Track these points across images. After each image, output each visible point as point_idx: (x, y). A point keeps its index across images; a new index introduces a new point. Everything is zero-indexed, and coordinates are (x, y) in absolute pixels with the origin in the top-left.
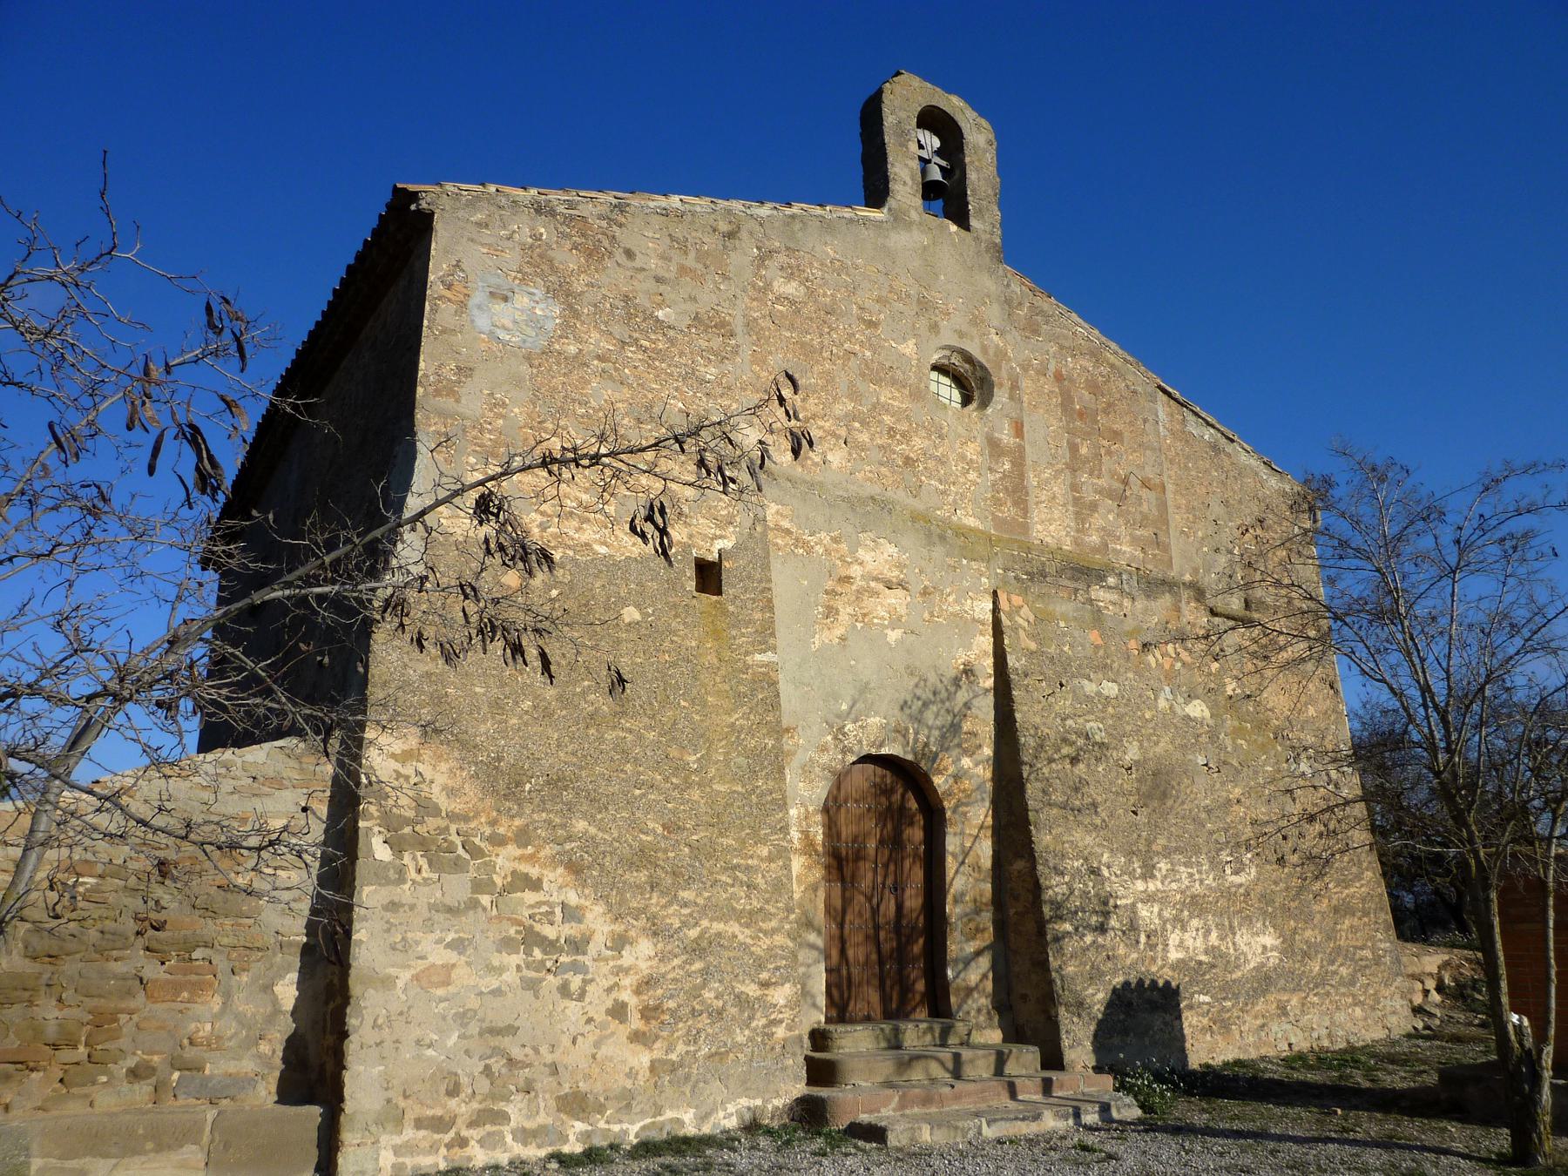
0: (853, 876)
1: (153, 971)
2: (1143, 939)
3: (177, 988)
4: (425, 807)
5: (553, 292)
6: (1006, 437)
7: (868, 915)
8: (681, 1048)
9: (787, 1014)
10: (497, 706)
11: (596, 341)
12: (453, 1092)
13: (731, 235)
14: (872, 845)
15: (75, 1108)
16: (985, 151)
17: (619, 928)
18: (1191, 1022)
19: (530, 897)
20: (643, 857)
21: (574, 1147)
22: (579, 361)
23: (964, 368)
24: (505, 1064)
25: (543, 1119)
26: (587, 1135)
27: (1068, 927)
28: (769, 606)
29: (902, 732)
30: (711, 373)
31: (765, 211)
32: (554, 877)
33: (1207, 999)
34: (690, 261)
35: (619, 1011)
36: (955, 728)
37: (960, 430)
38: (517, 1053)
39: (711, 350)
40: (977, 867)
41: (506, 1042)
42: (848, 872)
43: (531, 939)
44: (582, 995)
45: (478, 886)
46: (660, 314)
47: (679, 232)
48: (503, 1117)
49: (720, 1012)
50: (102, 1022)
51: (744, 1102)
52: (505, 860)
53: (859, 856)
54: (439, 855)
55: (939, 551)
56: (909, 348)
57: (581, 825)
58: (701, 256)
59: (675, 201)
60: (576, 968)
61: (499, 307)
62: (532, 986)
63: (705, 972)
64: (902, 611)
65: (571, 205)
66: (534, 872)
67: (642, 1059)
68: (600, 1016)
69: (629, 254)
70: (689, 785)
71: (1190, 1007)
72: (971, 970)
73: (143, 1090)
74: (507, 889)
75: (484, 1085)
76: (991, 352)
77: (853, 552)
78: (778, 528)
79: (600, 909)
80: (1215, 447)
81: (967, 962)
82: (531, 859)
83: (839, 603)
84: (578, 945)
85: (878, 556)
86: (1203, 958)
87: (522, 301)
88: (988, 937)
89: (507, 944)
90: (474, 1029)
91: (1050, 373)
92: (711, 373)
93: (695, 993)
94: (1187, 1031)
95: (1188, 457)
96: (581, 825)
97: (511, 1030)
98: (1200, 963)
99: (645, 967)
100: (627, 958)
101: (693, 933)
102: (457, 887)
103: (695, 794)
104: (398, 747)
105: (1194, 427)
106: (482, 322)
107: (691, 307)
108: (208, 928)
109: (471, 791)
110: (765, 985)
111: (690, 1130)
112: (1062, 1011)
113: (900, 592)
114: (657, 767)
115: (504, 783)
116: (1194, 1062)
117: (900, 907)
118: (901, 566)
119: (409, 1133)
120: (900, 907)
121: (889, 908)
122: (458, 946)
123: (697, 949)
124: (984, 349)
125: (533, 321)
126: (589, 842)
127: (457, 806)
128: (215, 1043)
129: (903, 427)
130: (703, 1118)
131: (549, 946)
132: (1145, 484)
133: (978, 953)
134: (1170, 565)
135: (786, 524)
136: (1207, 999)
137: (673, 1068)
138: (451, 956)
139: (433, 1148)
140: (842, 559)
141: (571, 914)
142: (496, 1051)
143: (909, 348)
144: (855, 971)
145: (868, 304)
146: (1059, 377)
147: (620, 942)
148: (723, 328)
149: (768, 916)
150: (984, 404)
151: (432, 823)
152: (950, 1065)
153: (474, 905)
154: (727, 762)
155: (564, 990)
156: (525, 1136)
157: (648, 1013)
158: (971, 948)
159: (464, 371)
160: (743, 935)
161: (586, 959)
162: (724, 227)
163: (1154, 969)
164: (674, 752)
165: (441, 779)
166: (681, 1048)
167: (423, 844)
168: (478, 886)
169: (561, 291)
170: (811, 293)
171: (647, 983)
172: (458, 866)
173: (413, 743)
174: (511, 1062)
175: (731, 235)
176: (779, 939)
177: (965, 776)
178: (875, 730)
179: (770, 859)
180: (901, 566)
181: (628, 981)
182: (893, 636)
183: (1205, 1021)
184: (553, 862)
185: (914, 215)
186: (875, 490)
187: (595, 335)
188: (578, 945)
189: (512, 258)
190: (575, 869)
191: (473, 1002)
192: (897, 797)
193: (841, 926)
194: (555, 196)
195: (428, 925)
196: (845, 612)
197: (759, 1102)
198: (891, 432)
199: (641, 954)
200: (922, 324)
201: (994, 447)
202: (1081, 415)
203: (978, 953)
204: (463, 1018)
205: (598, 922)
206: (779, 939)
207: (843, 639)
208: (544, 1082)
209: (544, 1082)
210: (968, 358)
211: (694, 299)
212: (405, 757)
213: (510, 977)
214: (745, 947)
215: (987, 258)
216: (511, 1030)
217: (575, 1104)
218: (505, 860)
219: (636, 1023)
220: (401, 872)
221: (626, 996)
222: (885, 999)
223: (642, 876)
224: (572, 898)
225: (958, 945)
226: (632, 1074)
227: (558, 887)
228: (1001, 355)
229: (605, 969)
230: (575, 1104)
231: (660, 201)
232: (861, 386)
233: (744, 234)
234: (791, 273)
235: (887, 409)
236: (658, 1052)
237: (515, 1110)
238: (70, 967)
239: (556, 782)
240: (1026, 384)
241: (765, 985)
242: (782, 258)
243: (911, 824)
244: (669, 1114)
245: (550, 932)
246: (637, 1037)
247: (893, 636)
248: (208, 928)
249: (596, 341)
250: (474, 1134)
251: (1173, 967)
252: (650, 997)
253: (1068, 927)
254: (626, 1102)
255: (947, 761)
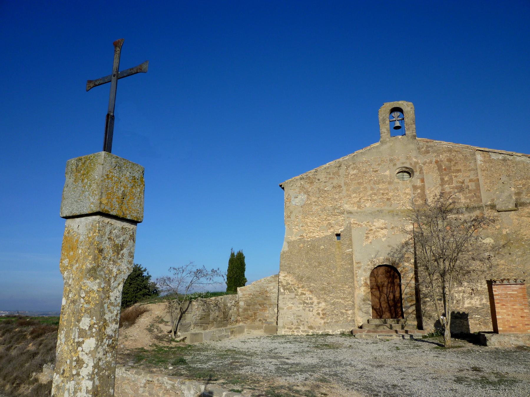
0: (382, 290)
1: (260, 307)
2: (455, 302)
3: (263, 310)
4: (288, 284)
5: (305, 193)
6: (419, 183)
7: (386, 298)
8: (330, 320)
9: (351, 315)
10: (299, 267)
11: (314, 199)
12: (292, 324)
13: (340, 166)
14: (386, 283)
15: (253, 324)
16: (410, 111)
17: (319, 301)
18: (471, 322)
19: (304, 296)
20: (323, 289)
21: (310, 334)
22: (311, 204)
23: (407, 170)
24: (300, 322)
25: (306, 329)
26: (312, 332)
27: (428, 299)
28: (351, 240)
29: (388, 259)
30: (337, 197)
31: (347, 158)
32: (308, 293)
33: (479, 316)
34: (331, 176)
35: (319, 314)
36: (403, 257)
37: (404, 187)
38: (302, 320)
39: (337, 192)
40: (410, 287)
41: (300, 318)
42: (381, 289)
43: (304, 303)
44: (312, 311)
45: (296, 295)
46: (326, 189)
47: (328, 171)
48: (300, 328)
49: (337, 315)
50: (255, 314)
51: (341, 330)
52: (300, 291)
53: (383, 286)
54: (290, 290)
55: (396, 218)
56: (387, 173)
57: (312, 284)
58: (333, 174)
59: (327, 165)
60: (312, 307)
61: (296, 199)
62: (304, 310)
63: (335, 308)
64: (386, 233)
65: (307, 175)
66: (305, 292)
67: (322, 321)
68: (315, 314)
69: (319, 180)
70: (332, 276)
71: (472, 318)
72: (409, 309)
73: (260, 323)
74: (301, 295)
75: (297, 324)
76: (413, 164)
77: (372, 223)
78: (354, 223)
79: (315, 298)
80: (504, 160)
81: (409, 307)
82: (304, 290)
83: (369, 235)
84: (312, 303)
85: (379, 223)
86: (479, 306)
87: (300, 197)
88: (414, 302)
89: (300, 303)
90: (295, 316)
91: (434, 162)
92: (337, 197)
93: (333, 311)
94: (470, 324)
95: (492, 167)
96: (312, 284)
97: (301, 316)
98: (477, 308)
99: (323, 307)
100: (320, 305)
101: (332, 301)
102: (293, 295)
103: (333, 277)
104: (284, 275)
105: (494, 156)
106: (294, 203)
107: (332, 185)
108: (265, 302)
109: (295, 280)
110: (347, 310)
111: (331, 333)
112: (424, 318)
113: (385, 230)
114: (326, 274)
115: (300, 279)
116: (472, 332)
117: (394, 296)
118: (385, 224)
119: (286, 329)
120: (394, 296)
121: (391, 296)
122: (293, 304)
123: (333, 304)
124: (411, 164)
125: (302, 200)
126: (314, 287)
127: (293, 283)
128: (268, 317)
129: (387, 192)
130: (333, 332)
131: (307, 304)
132: (471, 181)
133: (411, 305)
134: (481, 201)
135: (356, 222)
136: (479, 316)
137: (328, 323)
138: (292, 305)
139: (290, 332)
140: (370, 226)
141: (311, 299)
142: (299, 319)
143: (387, 173)
144: (383, 309)
145: (375, 167)
146: (437, 162)
147: (319, 303)
148: (340, 186)
149: (348, 298)
150: (413, 176)
151: (289, 286)
152: (389, 327)
153: (295, 298)
154: (340, 271)
155: (309, 310)
156: (303, 331)
157: (323, 314)
158: (409, 304)
159: (291, 213)
160: (342, 302)
161: (313, 306)
162: (338, 165)
163: (458, 309)
164: (330, 270)
165: (290, 279)
166: (330, 320)
167: (288, 289)
168: (296, 295)
169: (307, 193)
170: (360, 171)
171: (324, 310)
172: (293, 292)
173: (286, 274)
174: (301, 321)
175: (340, 166)
176: (350, 302)
177: (407, 267)
178: (381, 260)
179: (349, 288)
180: (385, 224)
181: (320, 309)
182: (383, 239)
183: (477, 322)
184: (308, 291)
185: (388, 140)
186: (379, 209)
187: (313, 198)
188: (312, 303)
189: (298, 190)
190: (311, 292)
191: (295, 312)
192: (392, 273)
193: (380, 300)
194: (304, 175)
195: (289, 301)
196: (371, 237)
197: (344, 330)
198: (383, 194)
199: (323, 305)
200: (391, 165)
201: (415, 188)
202: (445, 169)
203: (411, 305)
204: (294, 314)
205: (315, 300)
206: (350, 302)
207: (371, 242)
208: (306, 324)
209: (306, 324)
210: (407, 168)
211: (332, 183)
212: (285, 276)
213: (301, 308)
214: (343, 304)
215: (411, 140)
216: (301, 316)
217: (311, 327)
218: (300, 291)
219: (321, 316)
220: (285, 293)
221: (320, 311)
222: (392, 315)
223: (323, 292)
224: (311, 296)
225: (405, 304)
226: (320, 324)
227: (308, 294)
228: (417, 163)
229: (316, 307)
230: (311, 327)
231: (325, 166)
232: (374, 186)
233: (342, 165)
234: (354, 169)
235: (381, 189)
236: (325, 320)
237: (301, 328)
238: (251, 307)
239: (308, 278)
240: (424, 168)
241: (347, 310)
242: (352, 166)
243: (396, 278)
244: (327, 330)
245: (307, 301)
246: (321, 318)
247: (383, 239)
248: (265, 302)
249: (314, 199)
250: (295, 330)
251: (466, 309)
252: (324, 312)
253: (428, 299)
254: (319, 328)
255: (401, 264)
